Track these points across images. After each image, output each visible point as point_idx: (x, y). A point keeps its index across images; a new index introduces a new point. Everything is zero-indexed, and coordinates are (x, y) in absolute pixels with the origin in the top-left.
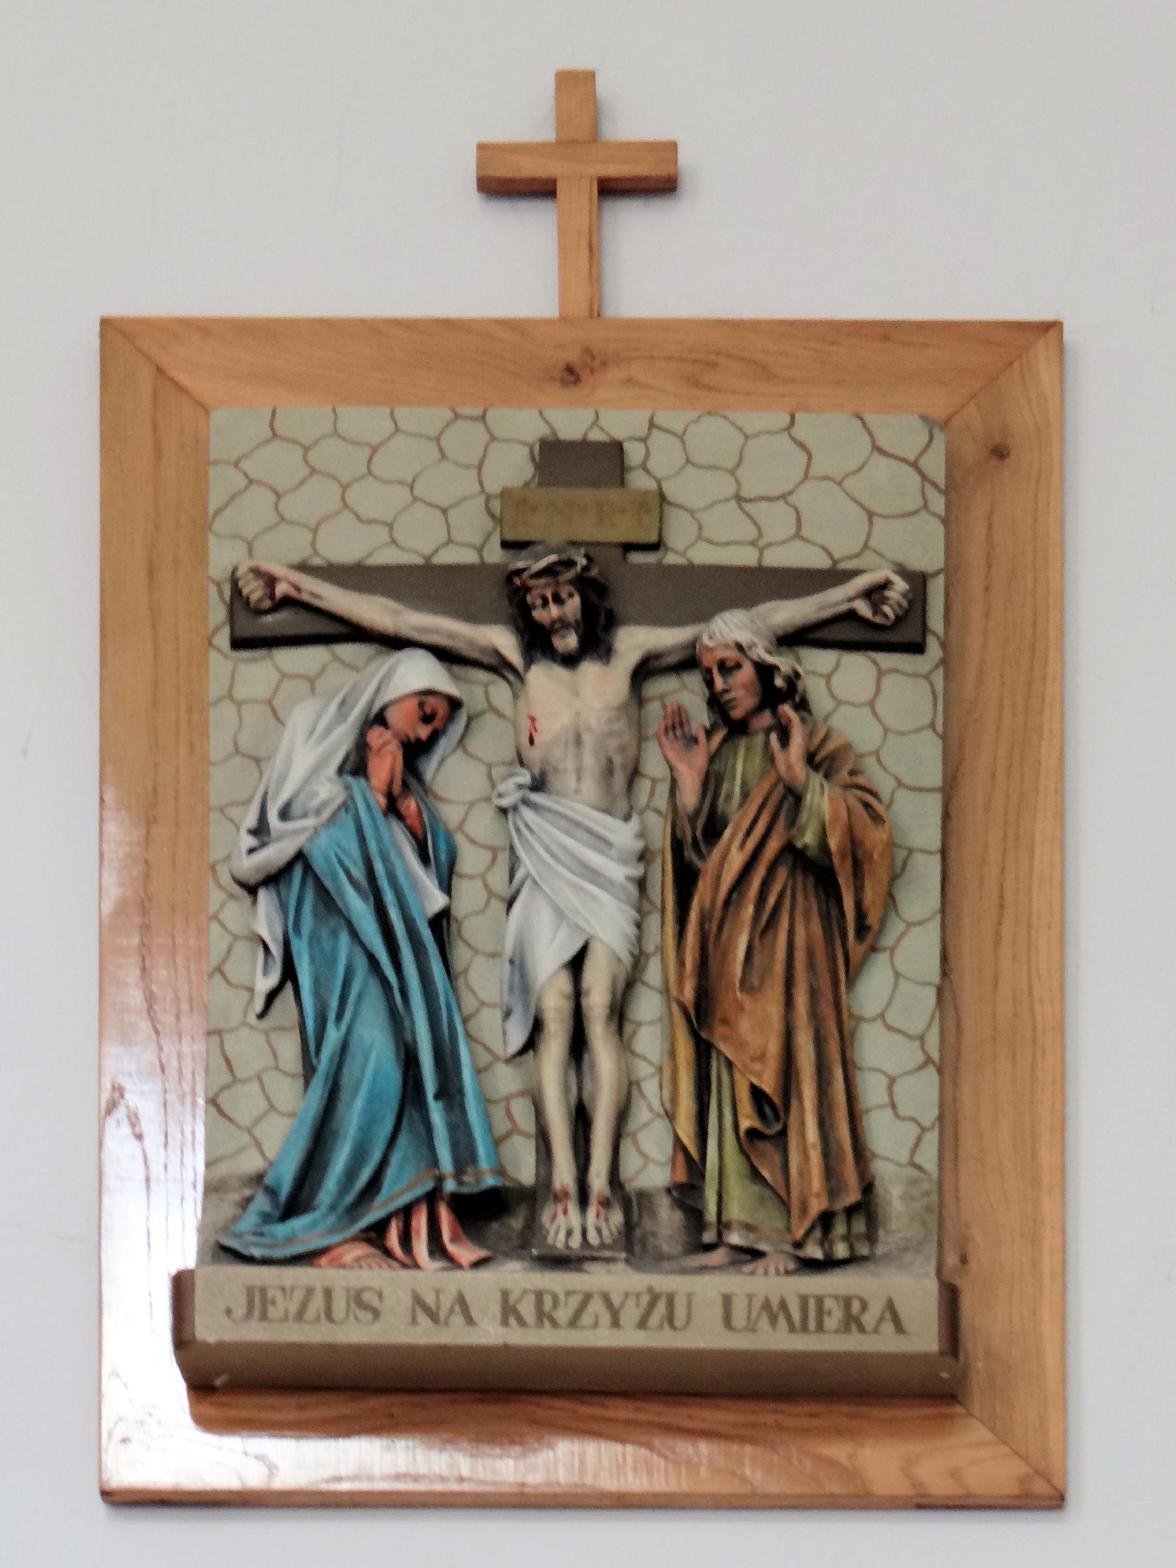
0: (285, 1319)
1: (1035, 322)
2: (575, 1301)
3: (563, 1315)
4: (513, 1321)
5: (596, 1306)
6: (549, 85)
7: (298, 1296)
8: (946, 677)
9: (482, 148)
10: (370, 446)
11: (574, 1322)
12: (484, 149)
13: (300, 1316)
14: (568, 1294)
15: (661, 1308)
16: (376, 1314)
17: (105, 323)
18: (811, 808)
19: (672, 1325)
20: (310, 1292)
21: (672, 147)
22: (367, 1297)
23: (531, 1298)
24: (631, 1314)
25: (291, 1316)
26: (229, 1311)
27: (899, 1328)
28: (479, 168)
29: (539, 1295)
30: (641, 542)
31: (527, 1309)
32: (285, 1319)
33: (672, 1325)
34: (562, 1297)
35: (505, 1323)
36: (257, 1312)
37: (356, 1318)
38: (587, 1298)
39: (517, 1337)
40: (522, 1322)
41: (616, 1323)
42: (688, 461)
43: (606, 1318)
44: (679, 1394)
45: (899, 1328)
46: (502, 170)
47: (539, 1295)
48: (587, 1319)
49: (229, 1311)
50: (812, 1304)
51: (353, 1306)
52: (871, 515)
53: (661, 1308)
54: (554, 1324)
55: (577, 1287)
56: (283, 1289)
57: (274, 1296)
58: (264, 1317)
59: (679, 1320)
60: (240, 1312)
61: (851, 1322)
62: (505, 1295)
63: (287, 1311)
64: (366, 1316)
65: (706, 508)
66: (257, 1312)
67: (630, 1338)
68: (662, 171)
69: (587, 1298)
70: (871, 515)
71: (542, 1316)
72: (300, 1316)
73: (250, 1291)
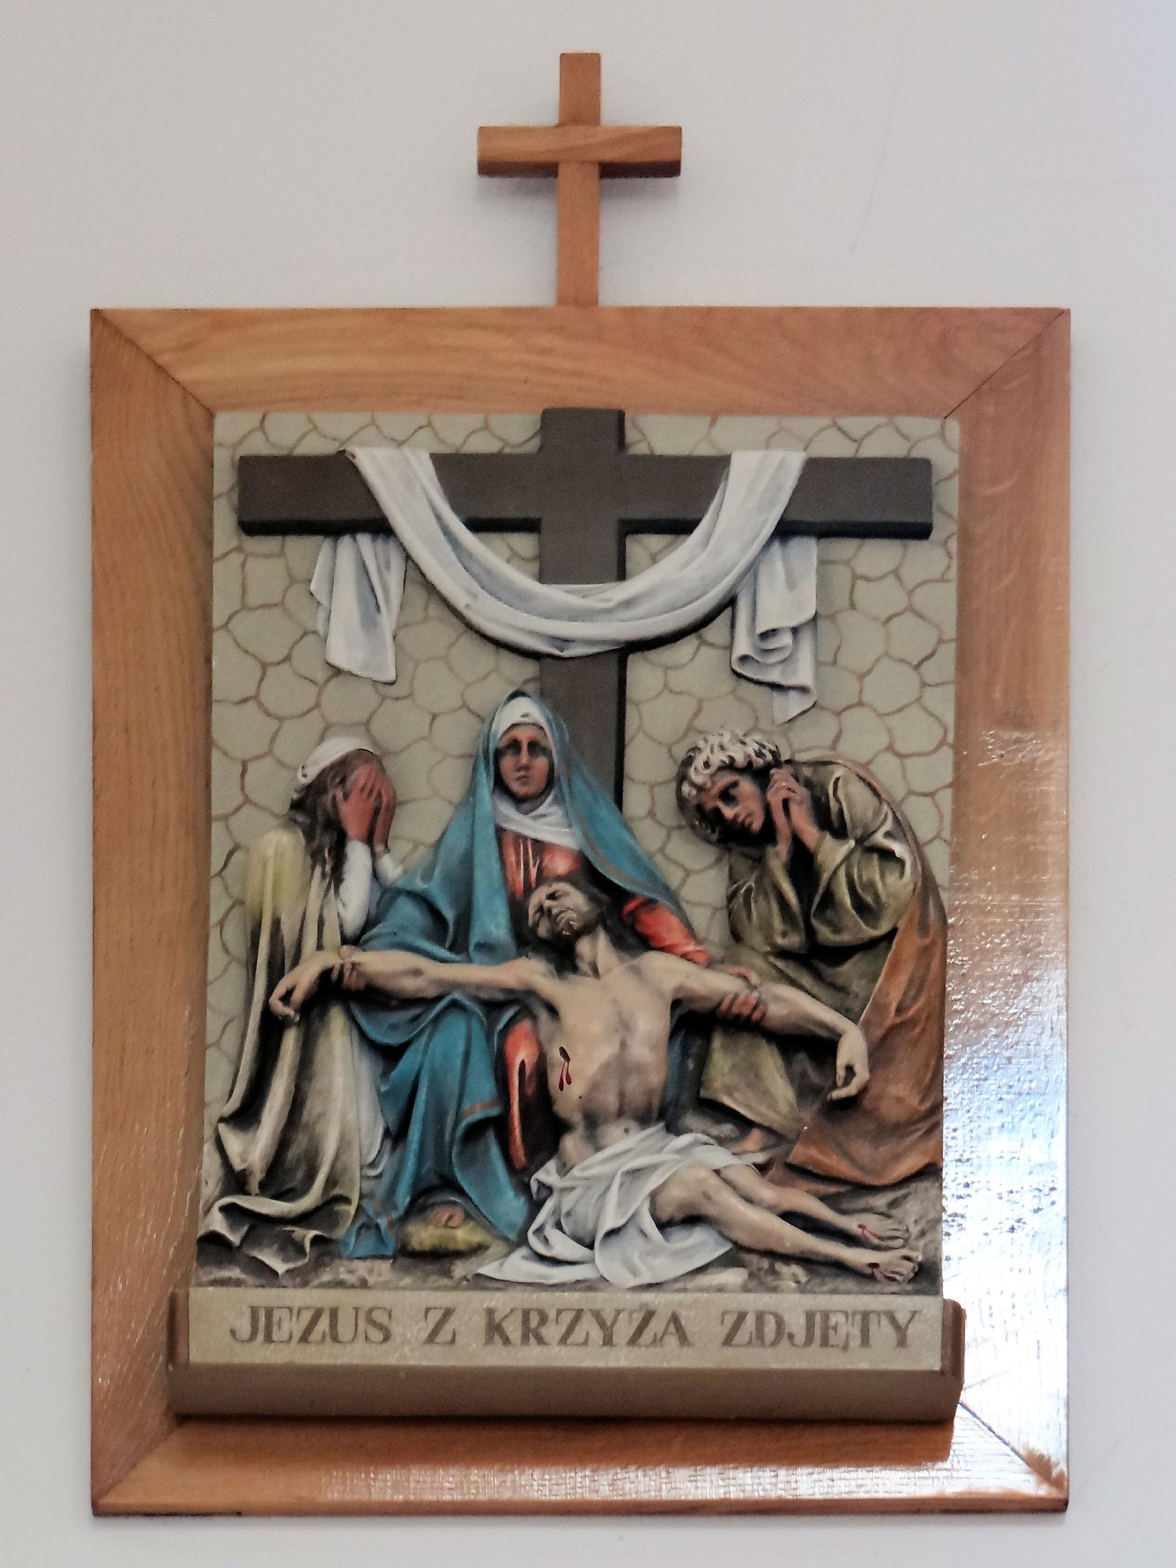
1: (93, 653)
2: (567, 1318)
4: (497, 1338)
5: (588, 1325)
7: (306, 1316)
8: (956, 800)
9: (485, 133)
12: (485, 133)
13: (305, 1338)
15: (324, 1324)
18: (766, 895)
19: (335, 1339)
20: (318, 1314)
23: (518, 1318)
24: (623, 1330)
25: (296, 1337)
27: (683, 1339)
29: (526, 1314)
31: (513, 1329)
34: (552, 1314)
35: (489, 1340)
36: (260, 1337)
37: (367, 1338)
38: (579, 1314)
39: (497, 1357)
40: (506, 1341)
41: (608, 1341)
42: (367, 723)
43: (597, 1335)
45: (683, 1339)
47: (526, 1314)
49: (233, 1332)
50: (818, 1318)
51: (362, 1324)
53: (324, 1324)
54: (540, 1340)
55: (438, 1304)
56: (290, 1309)
57: (837, 1323)
58: (268, 1338)
60: (244, 1327)
61: (531, 1335)
62: (490, 1312)
64: (376, 1335)
65: (647, 735)
66: (260, 1337)
67: (622, 1358)
68: (664, 155)
71: (494, 1329)
72: (305, 1338)
73: (254, 1311)
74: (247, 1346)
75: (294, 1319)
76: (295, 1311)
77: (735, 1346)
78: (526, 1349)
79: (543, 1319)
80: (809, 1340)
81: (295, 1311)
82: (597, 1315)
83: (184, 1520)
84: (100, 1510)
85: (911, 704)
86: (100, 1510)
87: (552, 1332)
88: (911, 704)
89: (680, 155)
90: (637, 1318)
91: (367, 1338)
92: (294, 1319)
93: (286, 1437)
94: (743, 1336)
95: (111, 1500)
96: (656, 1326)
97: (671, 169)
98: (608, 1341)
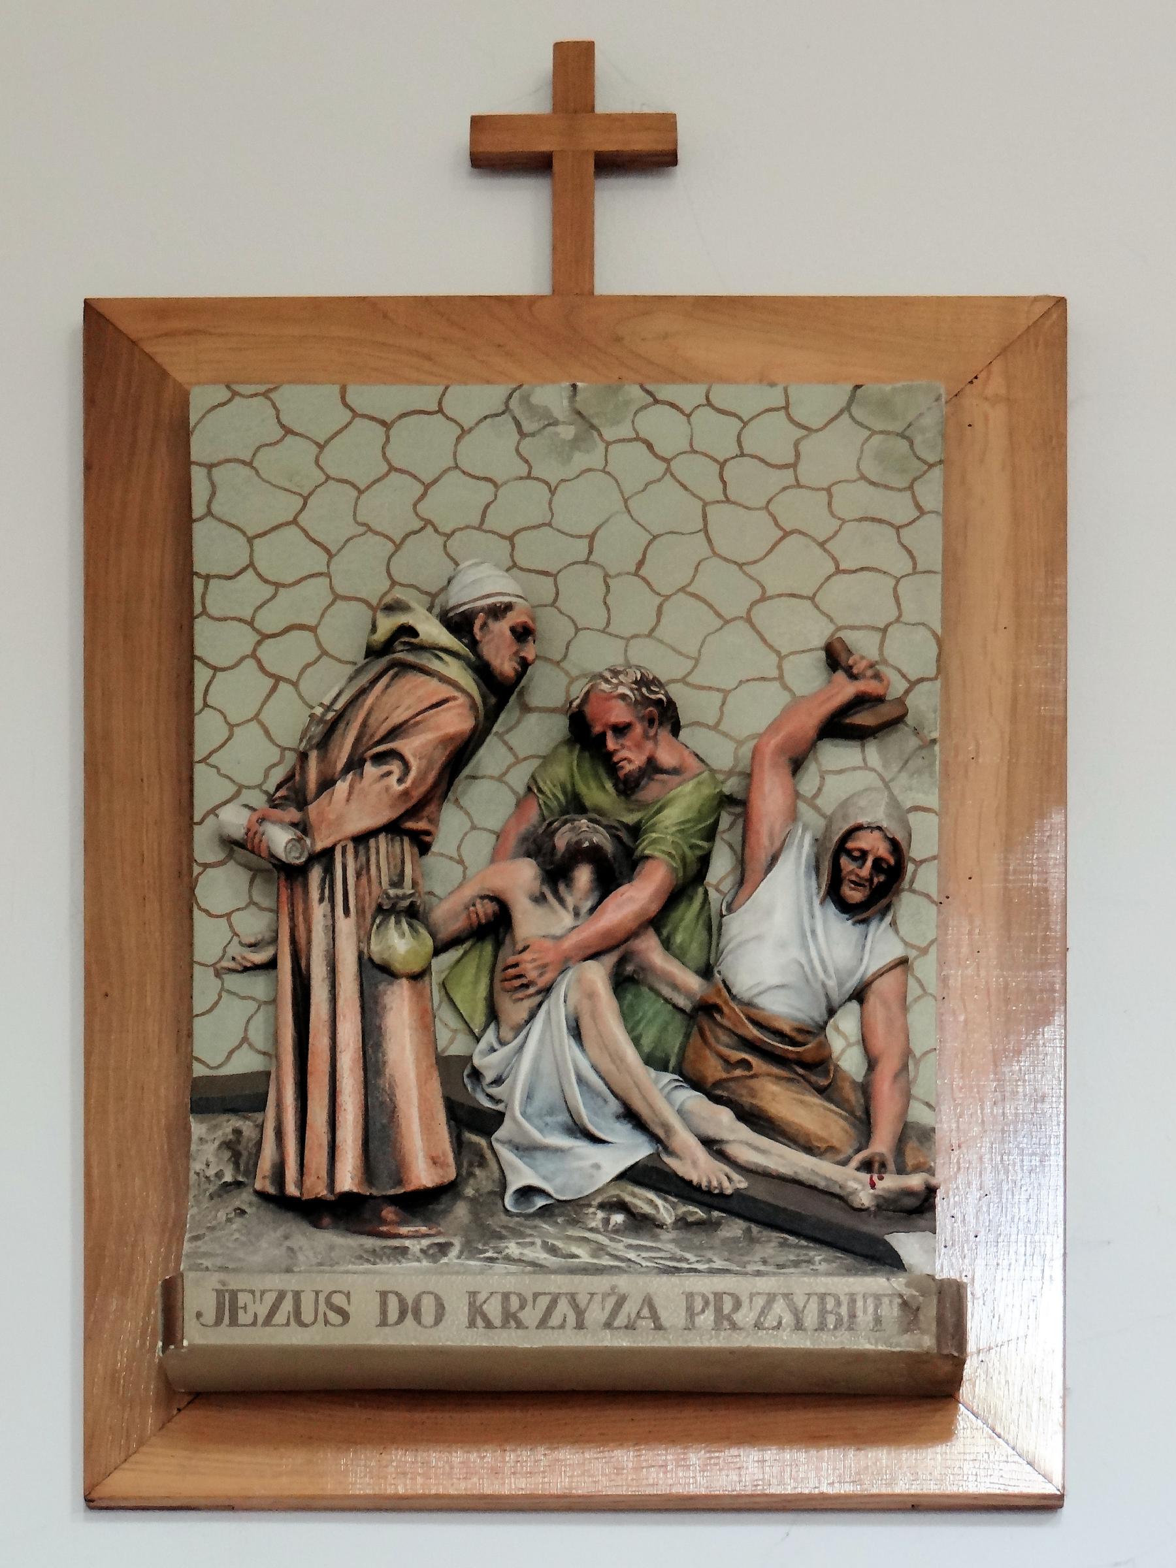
0: (254, 1324)
2: (543, 1302)
3: (530, 1316)
4: (480, 1322)
5: (563, 1306)
6: (546, 62)
7: (270, 1298)
9: (478, 123)
10: (637, 434)
11: (543, 1323)
12: (478, 123)
14: (536, 1296)
15: (287, 1305)
16: (345, 1315)
17: (1061, 302)
20: (281, 1296)
21: (667, 123)
22: (338, 1300)
25: (260, 1320)
26: (199, 1315)
28: (473, 141)
29: (506, 1297)
30: (82, 485)
31: (493, 1309)
32: (254, 1324)
33: (301, 1324)
35: (472, 1324)
36: (226, 1320)
37: (326, 1322)
39: (478, 1339)
40: (489, 1325)
41: (580, 1325)
43: (787, 1319)
44: (855, 1396)
45: (659, 1327)
46: (497, 144)
48: (555, 1320)
51: (322, 1307)
52: (727, 500)
53: (287, 1305)
54: (520, 1325)
58: (234, 1322)
59: (307, 1317)
60: (210, 1316)
61: (510, 1318)
62: (473, 1294)
63: (256, 1315)
64: (334, 1318)
66: (226, 1320)
68: (641, 143)
69: (771, 1298)
70: (727, 500)
71: (477, 1314)
74: (340, 1329)
75: (258, 1301)
76: (258, 1295)
77: (275, 1325)
78: (505, 1333)
79: (738, 1305)
80: (218, 1321)
81: (258, 1295)
82: (572, 1298)
83: (121, 1514)
84: (94, 1502)
85: (622, 638)
86: (94, 1502)
87: (745, 1317)
88: (622, 638)
89: (675, 142)
90: (611, 1302)
91: (326, 1322)
92: (258, 1301)
93: (646, 1416)
94: (280, 1318)
95: (121, 1483)
96: (630, 1308)
97: (674, 162)
98: (580, 1325)
